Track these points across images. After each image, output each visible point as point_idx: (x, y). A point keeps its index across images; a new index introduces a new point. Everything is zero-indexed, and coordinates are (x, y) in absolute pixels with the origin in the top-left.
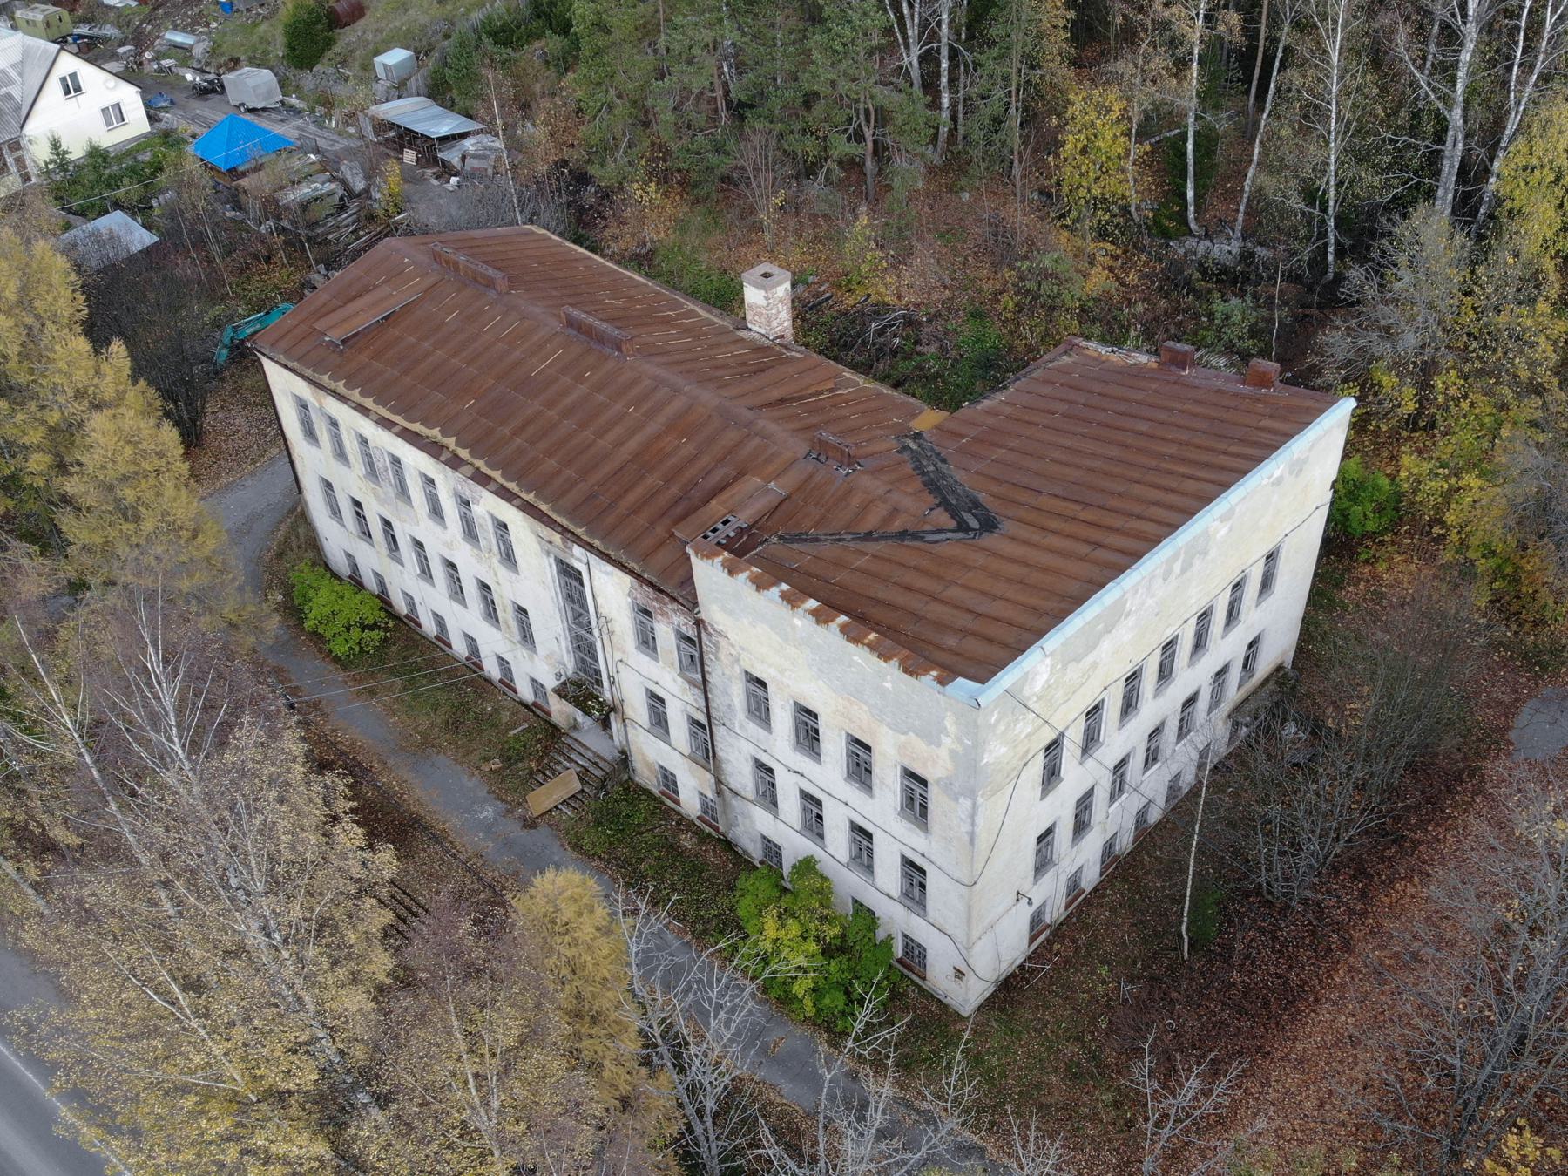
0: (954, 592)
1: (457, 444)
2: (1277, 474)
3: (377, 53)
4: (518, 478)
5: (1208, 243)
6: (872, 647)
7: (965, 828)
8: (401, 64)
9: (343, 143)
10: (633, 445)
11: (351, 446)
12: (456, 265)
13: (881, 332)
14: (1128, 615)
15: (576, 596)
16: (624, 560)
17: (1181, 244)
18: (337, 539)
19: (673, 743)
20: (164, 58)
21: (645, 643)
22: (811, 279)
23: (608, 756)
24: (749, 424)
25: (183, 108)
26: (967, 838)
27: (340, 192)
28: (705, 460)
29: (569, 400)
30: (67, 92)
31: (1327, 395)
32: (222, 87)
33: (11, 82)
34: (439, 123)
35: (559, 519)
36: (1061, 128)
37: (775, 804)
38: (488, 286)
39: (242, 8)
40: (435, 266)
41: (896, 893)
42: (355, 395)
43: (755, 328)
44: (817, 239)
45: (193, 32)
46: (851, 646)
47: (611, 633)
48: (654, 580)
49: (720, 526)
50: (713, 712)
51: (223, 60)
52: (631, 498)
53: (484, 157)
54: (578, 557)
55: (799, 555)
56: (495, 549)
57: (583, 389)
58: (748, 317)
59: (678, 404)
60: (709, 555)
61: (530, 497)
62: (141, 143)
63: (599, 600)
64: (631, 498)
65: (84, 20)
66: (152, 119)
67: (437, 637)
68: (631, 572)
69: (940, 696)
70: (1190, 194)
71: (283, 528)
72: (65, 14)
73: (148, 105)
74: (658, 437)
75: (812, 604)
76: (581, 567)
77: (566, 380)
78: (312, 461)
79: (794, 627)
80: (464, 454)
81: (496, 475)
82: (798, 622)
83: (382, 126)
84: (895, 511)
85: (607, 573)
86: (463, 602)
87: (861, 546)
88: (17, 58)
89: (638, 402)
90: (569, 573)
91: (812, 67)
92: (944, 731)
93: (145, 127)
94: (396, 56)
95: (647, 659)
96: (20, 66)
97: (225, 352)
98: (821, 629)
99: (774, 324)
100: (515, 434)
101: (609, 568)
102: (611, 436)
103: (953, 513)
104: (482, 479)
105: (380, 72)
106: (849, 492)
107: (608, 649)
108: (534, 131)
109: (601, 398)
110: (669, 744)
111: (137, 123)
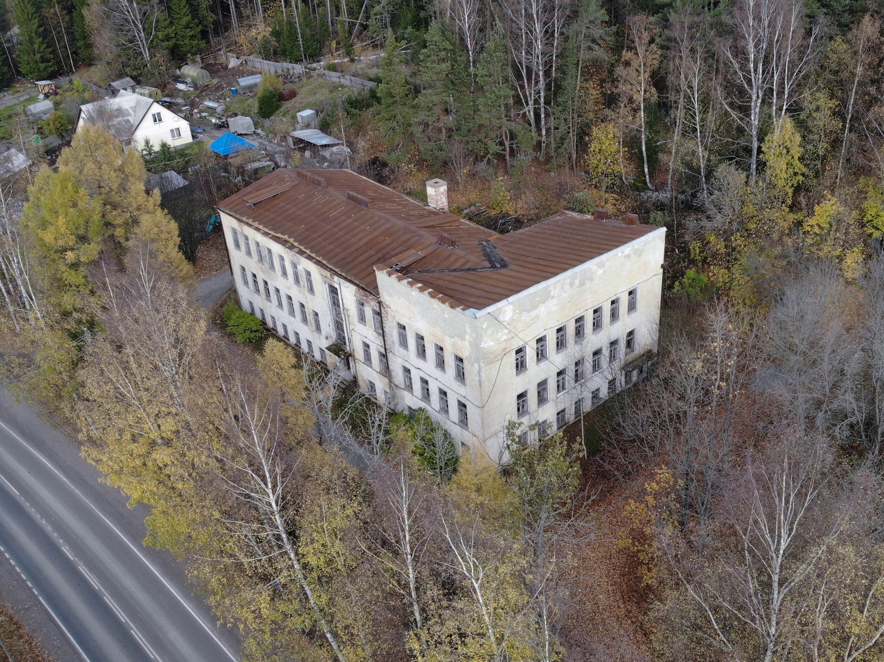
0: (481, 286)
1: (294, 241)
2: (626, 252)
3: (299, 111)
4: (317, 253)
5: (657, 193)
6: (439, 299)
7: (477, 379)
8: (309, 116)
9: (279, 149)
10: (365, 240)
11: (253, 247)
12: (306, 176)
13: (503, 224)
14: (553, 297)
15: (336, 302)
16: (353, 279)
17: (646, 194)
18: (246, 294)
19: (373, 366)
20: (203, 112)
21: (362, 319)
22: (477, 204)
23: (348, 379)
24: (415, 232)
25: (208, 132)
26: (478, 383)
27: (273, 166)
28: (394, 245)
29: (343, 225)
30: (155, 121)
31: (657, 225)
32: (228, 125)
33: (130, 115)
34: (321, 139)
35: (329, 266)
36: (590, 141)
37: (412, 388)
38: (318, 185)
39: (241, 92)
40: (298, 178)
41: (457, 421)
42: (256, 224)
43: (432, 205)
44: (483, 189)
45: (218, 102)
46: (432, 300)
47: (349, 316)
48: (364, 286)
49: (394, 266)
50: (387, 347)
51: (229, 114)
52: (361, 258)
53: (341, 154)
54: (337, 281)
55: (426, 276)
56: (306, 285)
57: (350, 221)
58: (429, 201)
59: (387, 226)
60: (380, 269)
61: (320, 259)
62: (188, 146)
63: (344, 301)
64: (361, 258)
65: (168, 96)
66: (194, 137)
67: (284, 336)
68: (355, 284)
69: (463, 316)
70: (646, 170)
71: (225, 296)
72: (159, 91)
73: (192, 131)
74: (377, 237)
75: (420, 285)
76: (337, 286)
77: (344, 218)
78: (237, 257)
79: (412, 296)
80: (296, 244)
81: (308, 251)
82: (414, 293)
83: (300, 141)
84: (468, 261)
85: (347, 287)
86: (294, 316)
87: (451, 273)
88: (133, 105)
89: (371, 226)
90: (333, 291)
91: (479, 113)
92: (466, 332)
93: (189, 139)
94: (308, 112)
95: (362, 326)
96: (134, 109)
97: (211, 227)
98: (421, 294)
99: (439, 203)
100: (319, 237)
101: (348, 284)
102: (357, 237)
103: (490, 260)
104: (301, 253)
105: (299, 119)
106: (450, 255)
107: (348, 325)
108: (362, 144)
109: (356, 224)
110: (372, 368)
111: (186, 137)
